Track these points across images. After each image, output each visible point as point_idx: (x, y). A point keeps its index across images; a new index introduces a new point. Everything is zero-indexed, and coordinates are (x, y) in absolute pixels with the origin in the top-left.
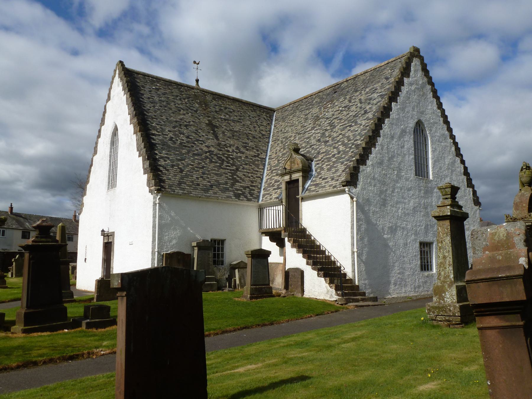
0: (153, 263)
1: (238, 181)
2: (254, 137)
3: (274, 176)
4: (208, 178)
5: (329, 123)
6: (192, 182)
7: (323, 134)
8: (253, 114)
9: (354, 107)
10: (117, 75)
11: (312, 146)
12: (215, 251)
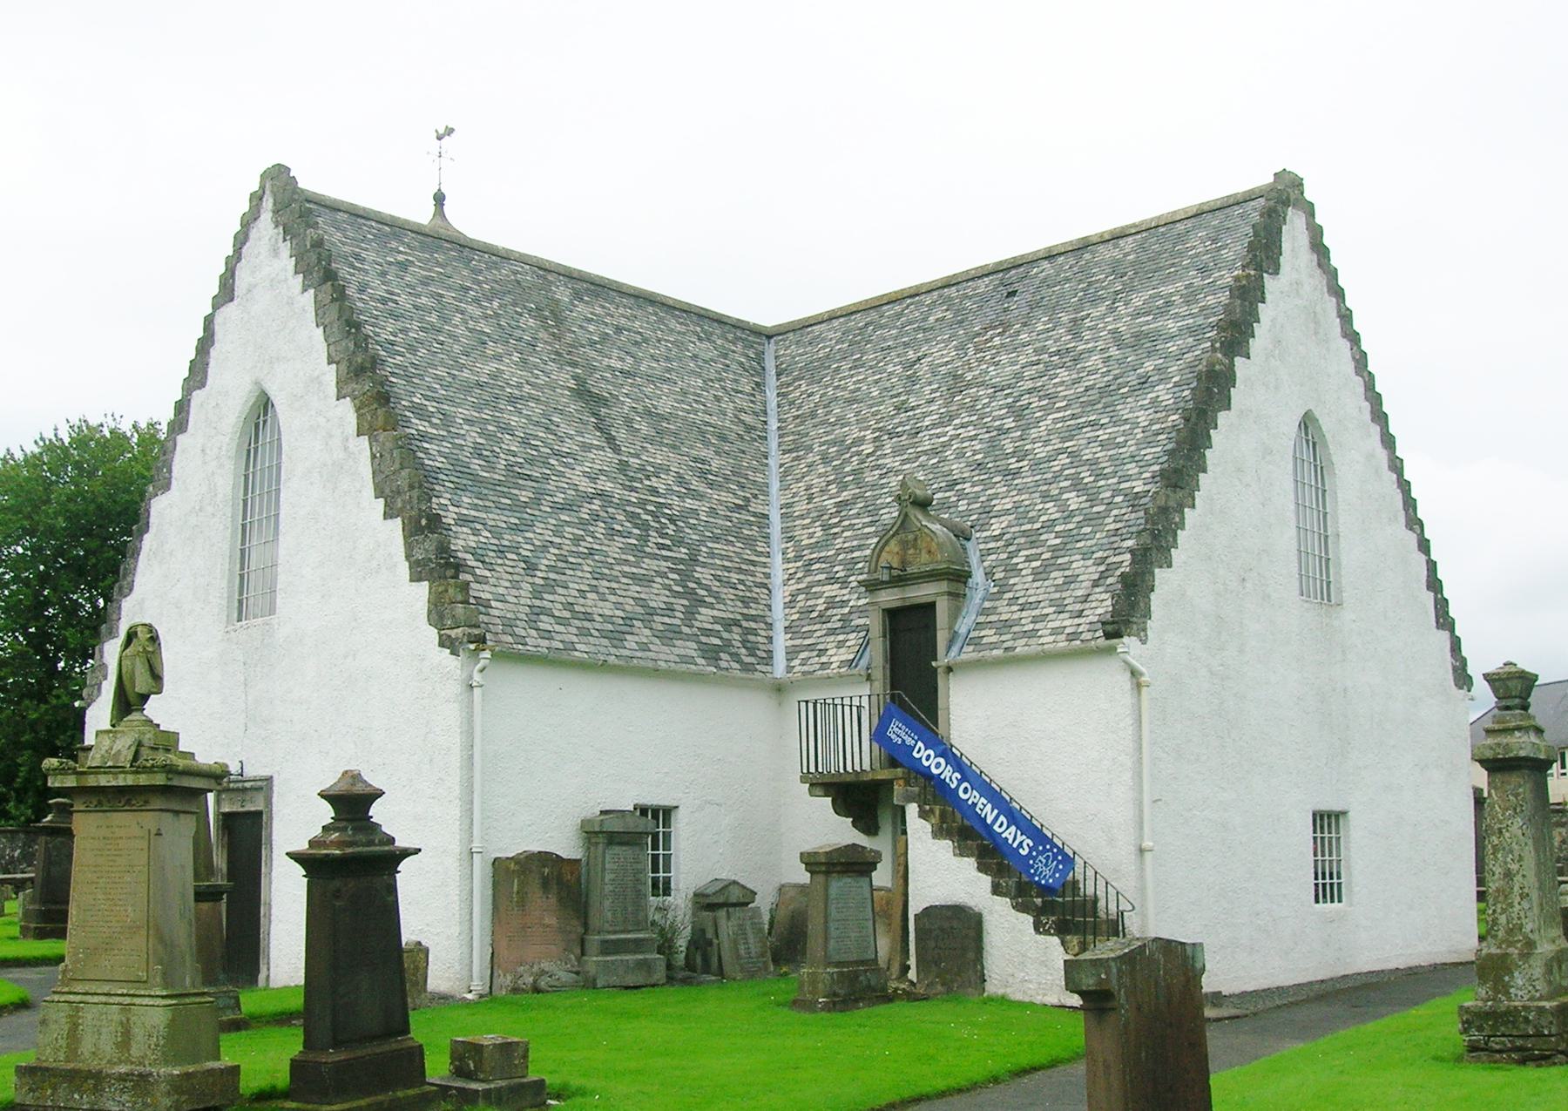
1: (702, 602)
2: (723, 438)
4: (613, 591)
5: (1009, 406)
7: (993, 444)
8: (705, 350)
10: (266, 216)
12: (655, 847)
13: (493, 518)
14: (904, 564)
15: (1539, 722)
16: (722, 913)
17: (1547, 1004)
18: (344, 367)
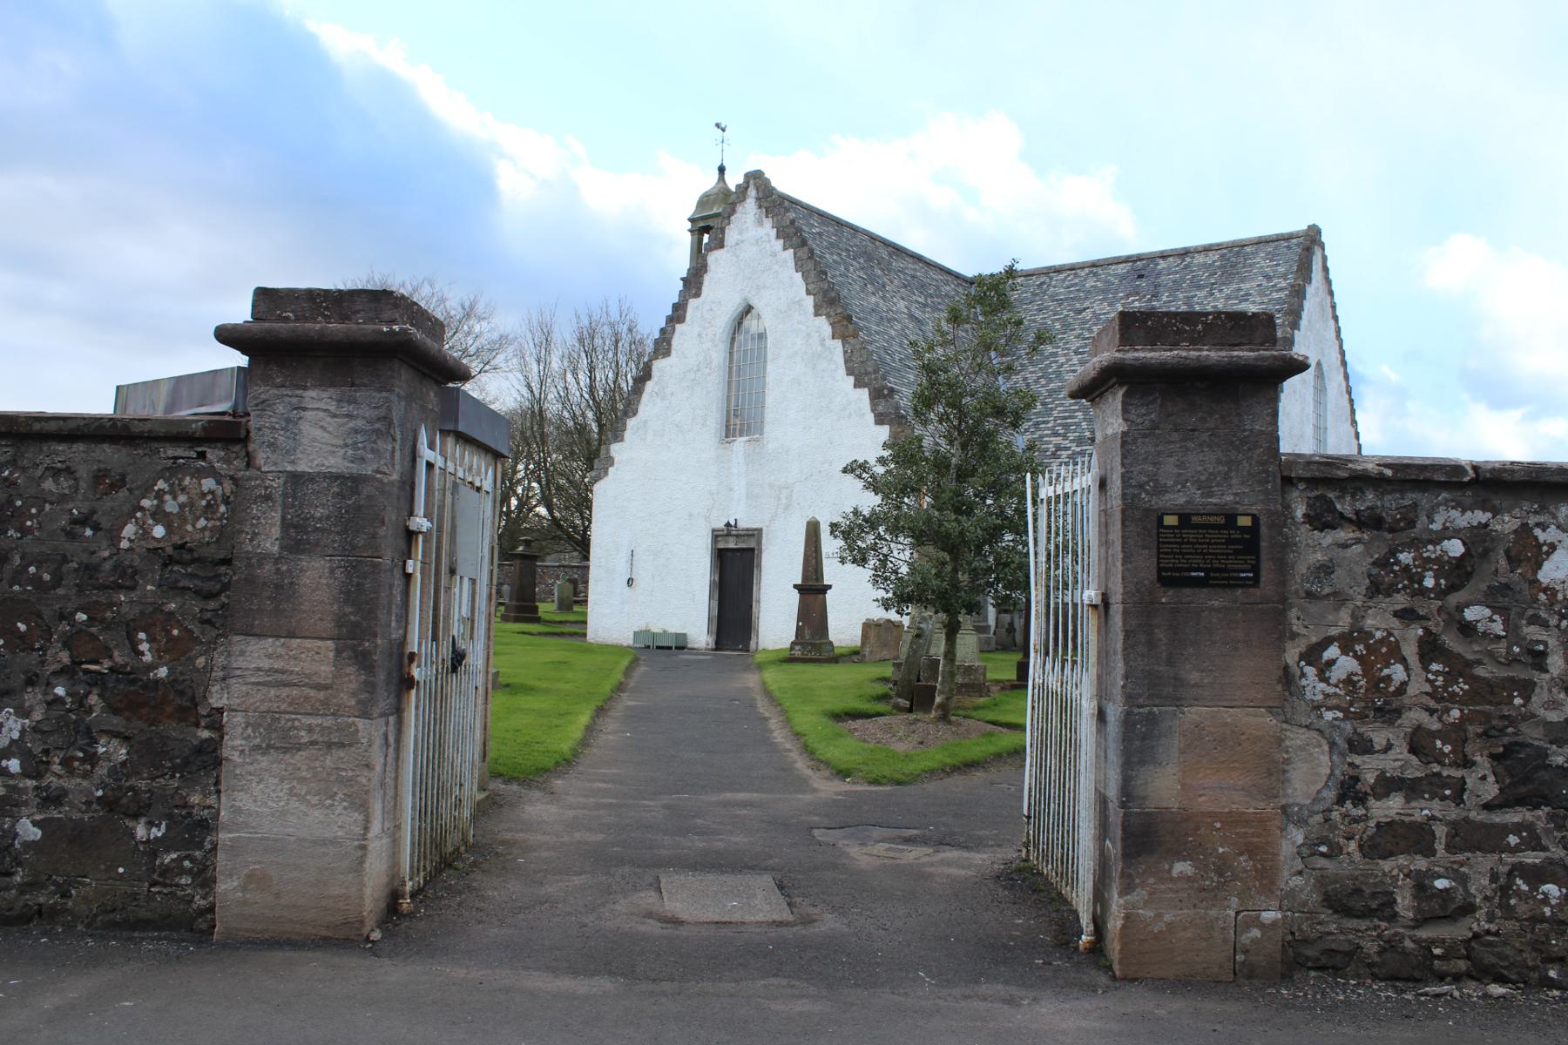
18: (820, 297)
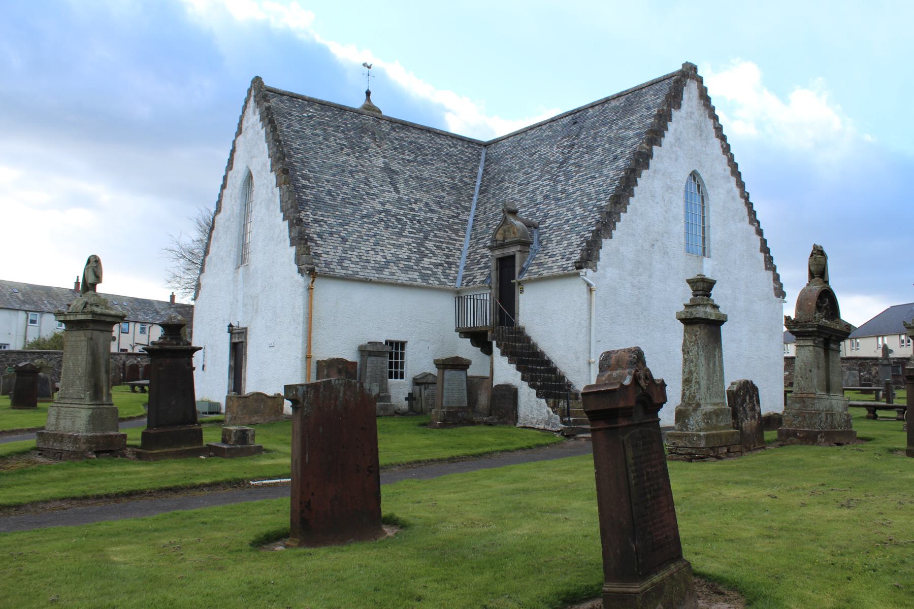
0: (308, 376)
1: (426, 256)
3: (480, 248)
4: (382, 251)
6: (359, 257)
9: (600, 149)
10: (252, 99)
11: (537, 204)
12: (391, 358)
13: (330, 221)
14: (505, 238)
15: (716, 302)
16: (423, 387)
17: (702, 433)
